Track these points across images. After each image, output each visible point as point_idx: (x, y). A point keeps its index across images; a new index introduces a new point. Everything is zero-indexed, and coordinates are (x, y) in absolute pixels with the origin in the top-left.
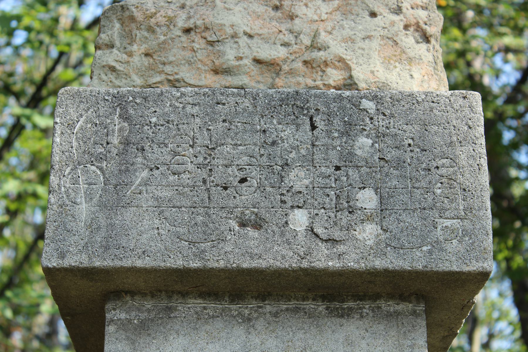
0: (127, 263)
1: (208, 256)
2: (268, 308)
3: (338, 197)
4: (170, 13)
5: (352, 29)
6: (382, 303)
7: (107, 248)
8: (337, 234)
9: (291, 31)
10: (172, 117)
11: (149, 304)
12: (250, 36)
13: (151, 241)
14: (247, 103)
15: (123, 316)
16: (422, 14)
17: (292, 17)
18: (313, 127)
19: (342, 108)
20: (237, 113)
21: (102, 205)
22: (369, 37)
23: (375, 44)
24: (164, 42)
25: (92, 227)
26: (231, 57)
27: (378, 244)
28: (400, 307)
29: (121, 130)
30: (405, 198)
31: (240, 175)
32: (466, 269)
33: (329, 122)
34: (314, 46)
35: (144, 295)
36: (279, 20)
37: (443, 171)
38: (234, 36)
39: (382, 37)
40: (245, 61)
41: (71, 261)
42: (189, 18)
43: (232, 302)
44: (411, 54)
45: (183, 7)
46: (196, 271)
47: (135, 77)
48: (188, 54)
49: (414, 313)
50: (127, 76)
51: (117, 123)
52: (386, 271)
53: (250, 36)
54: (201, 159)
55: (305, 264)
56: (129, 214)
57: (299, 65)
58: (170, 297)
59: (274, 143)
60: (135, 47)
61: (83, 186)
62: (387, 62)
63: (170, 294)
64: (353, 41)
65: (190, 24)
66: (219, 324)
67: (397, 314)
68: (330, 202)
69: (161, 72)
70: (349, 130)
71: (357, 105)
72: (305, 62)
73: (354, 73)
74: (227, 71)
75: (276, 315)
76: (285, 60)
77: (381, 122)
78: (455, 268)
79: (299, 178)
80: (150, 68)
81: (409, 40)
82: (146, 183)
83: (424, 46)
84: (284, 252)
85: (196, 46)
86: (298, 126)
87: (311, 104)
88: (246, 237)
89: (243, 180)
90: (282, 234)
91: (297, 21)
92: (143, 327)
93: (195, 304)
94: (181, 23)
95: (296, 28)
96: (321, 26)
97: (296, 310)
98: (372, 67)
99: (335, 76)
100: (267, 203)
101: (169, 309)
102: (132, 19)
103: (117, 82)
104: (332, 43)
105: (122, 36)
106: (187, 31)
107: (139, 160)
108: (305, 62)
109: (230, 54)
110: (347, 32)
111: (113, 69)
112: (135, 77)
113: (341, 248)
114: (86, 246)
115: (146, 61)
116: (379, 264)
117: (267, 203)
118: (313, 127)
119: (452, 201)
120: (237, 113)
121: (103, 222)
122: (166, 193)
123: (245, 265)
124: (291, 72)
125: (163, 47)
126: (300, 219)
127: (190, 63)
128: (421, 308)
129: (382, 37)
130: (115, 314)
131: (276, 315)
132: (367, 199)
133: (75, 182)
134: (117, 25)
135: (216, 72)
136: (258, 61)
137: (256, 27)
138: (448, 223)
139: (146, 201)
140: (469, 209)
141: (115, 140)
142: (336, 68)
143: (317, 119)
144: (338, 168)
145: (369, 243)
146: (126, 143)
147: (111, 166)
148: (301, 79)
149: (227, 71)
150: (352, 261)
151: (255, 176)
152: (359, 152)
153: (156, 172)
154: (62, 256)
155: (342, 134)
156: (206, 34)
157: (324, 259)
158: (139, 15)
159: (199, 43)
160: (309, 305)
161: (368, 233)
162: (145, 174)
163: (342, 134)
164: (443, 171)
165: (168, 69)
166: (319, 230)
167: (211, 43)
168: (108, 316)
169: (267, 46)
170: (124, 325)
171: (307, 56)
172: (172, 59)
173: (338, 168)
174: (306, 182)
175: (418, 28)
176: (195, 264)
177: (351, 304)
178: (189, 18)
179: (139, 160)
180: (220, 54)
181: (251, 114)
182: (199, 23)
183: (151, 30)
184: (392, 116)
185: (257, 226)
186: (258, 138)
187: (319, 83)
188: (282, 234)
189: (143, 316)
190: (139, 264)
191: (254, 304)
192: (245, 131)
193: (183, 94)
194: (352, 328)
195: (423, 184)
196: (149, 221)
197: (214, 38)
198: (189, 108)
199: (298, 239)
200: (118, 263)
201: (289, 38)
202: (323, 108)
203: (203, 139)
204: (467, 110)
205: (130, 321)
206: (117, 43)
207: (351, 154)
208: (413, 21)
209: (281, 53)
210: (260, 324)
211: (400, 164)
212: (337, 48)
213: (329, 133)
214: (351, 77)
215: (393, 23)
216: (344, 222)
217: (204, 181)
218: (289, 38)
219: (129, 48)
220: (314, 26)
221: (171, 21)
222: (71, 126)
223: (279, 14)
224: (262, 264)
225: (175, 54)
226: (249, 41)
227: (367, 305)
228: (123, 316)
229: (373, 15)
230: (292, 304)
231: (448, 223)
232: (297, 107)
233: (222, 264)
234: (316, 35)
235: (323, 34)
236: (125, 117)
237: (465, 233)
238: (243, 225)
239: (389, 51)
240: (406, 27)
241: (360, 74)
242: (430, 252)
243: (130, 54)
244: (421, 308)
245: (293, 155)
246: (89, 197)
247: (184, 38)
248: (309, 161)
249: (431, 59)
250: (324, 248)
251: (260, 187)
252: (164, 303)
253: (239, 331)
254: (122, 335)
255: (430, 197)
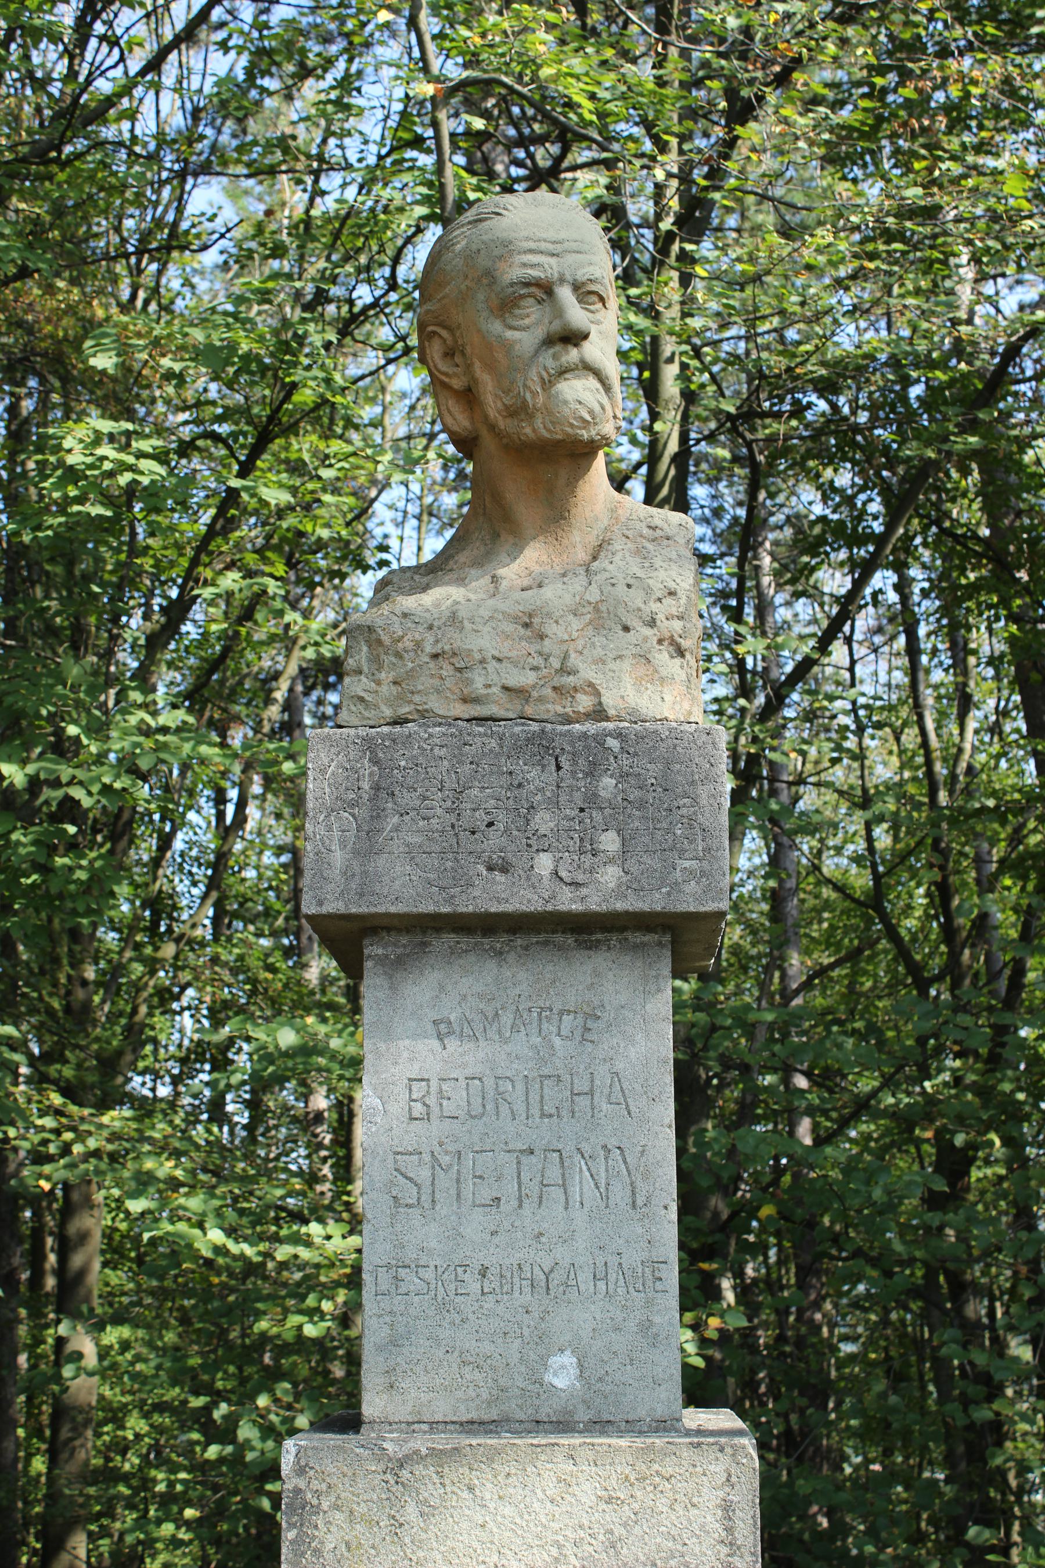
0: (381, 909)
1: (457, 901)
2: (519, 942)
3: (581, 840)
4: (417, 637)
5: (604, 647)
6: (629, 935)
7: (362, 895)
8: (580, 878)
9: (540, 654)
10: (421, 760)
11: (404, 940)
12: (499, 660)
13: (402, 886)
14: (494, 743)
15: (380, 951)
16: (677, 625)
17: (542, 637)
18: (559, 768)
19: (587, 747)
20: (484, 754)
21: (356, 853)
22: (620, 657)
23: (626, 665)
24: (412, 670)
25: (347, 874)
26: (479, 685)
27: (619, 886)
28: (646, 938)
29: (371, 774)
30: (646, 839)
31: (487, 819)
32: (702, 909)
33: (575, 763)
34: (564, 670)
35: (399, 930)
36: (528, 640)
37: (684, 811)
38: (483, 661)
39: (634, 656)
40: (495, 690)
41: (328, 908)
42: (437, 641)
43: (484, 936)
44: (664, 672)
45: (431, 627)
46: (447, 916)
47: (384, 708)
48: (436, 682)
49: (660, 944)
50: (376, 707)
51: (367, 767)
52: (627, 913)
53: (499, 660)
54: (449, 803)
55: (550, 908)
56: (381, 861)
57: (548, 691)
58: (424, 932)
59: (520, 785)
60: (383, 675)
61: (336, 834)
62: (638, 683)
63: (424, 930)
64: (604, 663)
65: (438, 649)
66: (472, 958)
67: (644, 945)
68: (574, 845)
69: (410, 702)
70: (593, 771)
71: (602, 743)
72: (555, 688)
73: (604, 699)
74: (476, 700)
75: (526, 948)
76: (534, 686)
77: (625, 761)
78: (692, 909)
79: (544, 822)
80: (400, 697)
81: (662, 657)
82: (397, 829)
83: (678, 661)
84: (530, 896)
85: (444, 673)
86: (543, 766)
87: (555, 744)
88: (494, 882)
89: (490, 824)
90: (528, 879)
91: (547, 642)
92: (400, 963)
93: (449, 939)
94: (429, 649)
95: (546, 650)
96: (572, 645)
97: (546, 943)
98: (622, 692)
99: (585, 702)
100: (513, 847)
101: (424, 944)
102: (379, 642)
103: (366, 714)
104: (581, 666)
105: (369, 660)
106: (435, 656)
107: (390, 805)
108: (555, 688)
109: (479, 682)
110: (599, 652)
111: (362, 699)
112: (384, 708)
113: (584, 891)
114: (342, 893)
115: (394, 689)
116: (620, 906)
117: (513, 847)
118: (559, 768)
119: (691, 842)
120: (484, 754)
121: (357, 870)
122: (416, 839)
123: (493, 910)
124: (541, 700)
125: (411, 674)
126: (545, 863)
127: (438, 691)
128: (668, 938)
129: (634, 656)
130: (373, 949)
131: (526, 948)
132: (610, 842)
133: (330, 829)
134: (365, 649)
135: (465, 700)
136: (506, 688)
137: (505, 648)
138: (687, 864)
139: (397, 846)
140: (708, 850)
141: (366, 786)
142: (585, 693)
143: (562, 759)
144: (582, 810)
145: (611, 885)
146: (377, 788)
147: (362, 812)
148: (550, 706)
149: (476, 700)
150: (595, 903)
151: (502, 819)
152: (603, 793)
153: (406, 818)
154: (320, 903)
155: (587, 775)
156: (454, 660)
157: (568, 902)
158: (386, 639)
159: (447, 671)
160: (559, 938)
161: (610, 876)
162: (396, 819)
163: (587, 775)
164: (684, 811)
165: (417, 698)
166: (563, 874)
167: (459, 670)
168: (366, 952)
169: (515, 671)
170: (382, 960)
171: (557, 681)
172: (420, 687)
173: (582, 810)
174: (552, 825)
175: (673, 642)
176: (446, 909)
177: (599, 936)
178: (437, 641)
179: (390, 805)
180: (469, 682)
181: (497, 755)
182: (447, 648)
183: (398, 655)
184: (636, 754)
185: (504, 870)
186: (505, 780)
187: (568, 710)
188: (528, 879)
189: (399, 951)
190: (393, 909)
191: (505, 938)
192: (492, 773)
193: (431, 735)
194: (600, 960)
195: (665, 825)
196: (402, 867)
197: (462, 665)
198: (436, 750)
199: (542, 883)
200: (373, 910)
201: (539, 661)
202: (568, 748)
203: (450, 783)
204: (710, 747)
205: (387, 956)
206: (366, 669)
207: (596, 795)
208: (667, 635)
209: (528, 679)
210: (512, 957)
211: (642, 805)
212: (588, 672)
213: (573, 773)
214: (600, 703)
215: (646, 639)
216: (587, 866)
217: (453, 826)
218: (539, 661)
219: (378, 676)
220: (564, 647)
221: (418, 645)
222: (323, 771)
223: (529, 633)
224: (508, 908)
225: (424, 682)
226: (497, 665)
227: (615, 937)
228: (380, 951)
229: (626, 629)
230: (542, 937)
231: (687, 864)
232: (543, 747)
233: (471, 909)
234: (566, 657)
235: (573, 655)
236: (375, 761)
237: (703, 873)
238: (490, 869)
239: (642, 670)
240: (660, 642)
241: (610, 701)
242: (669, 894)
243: (378, 683)
244: (668, 938)
245: (539, 797)
246: (343, 845)
247: (432, 665)
248: (555, 803)
249: (684, 677)
250: (567, 892)
251: (507, 830)
252: (418, 939)
253: (491, 965)
254: (380, 970)
255: (670, 838)
